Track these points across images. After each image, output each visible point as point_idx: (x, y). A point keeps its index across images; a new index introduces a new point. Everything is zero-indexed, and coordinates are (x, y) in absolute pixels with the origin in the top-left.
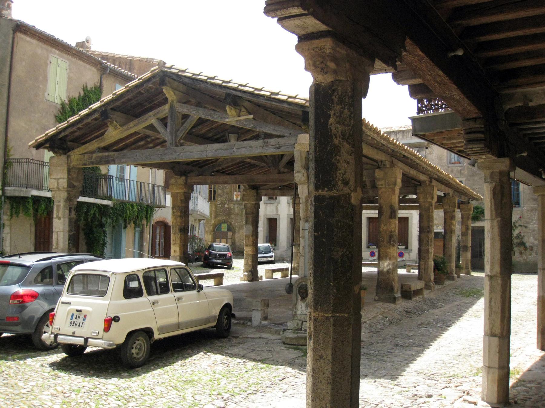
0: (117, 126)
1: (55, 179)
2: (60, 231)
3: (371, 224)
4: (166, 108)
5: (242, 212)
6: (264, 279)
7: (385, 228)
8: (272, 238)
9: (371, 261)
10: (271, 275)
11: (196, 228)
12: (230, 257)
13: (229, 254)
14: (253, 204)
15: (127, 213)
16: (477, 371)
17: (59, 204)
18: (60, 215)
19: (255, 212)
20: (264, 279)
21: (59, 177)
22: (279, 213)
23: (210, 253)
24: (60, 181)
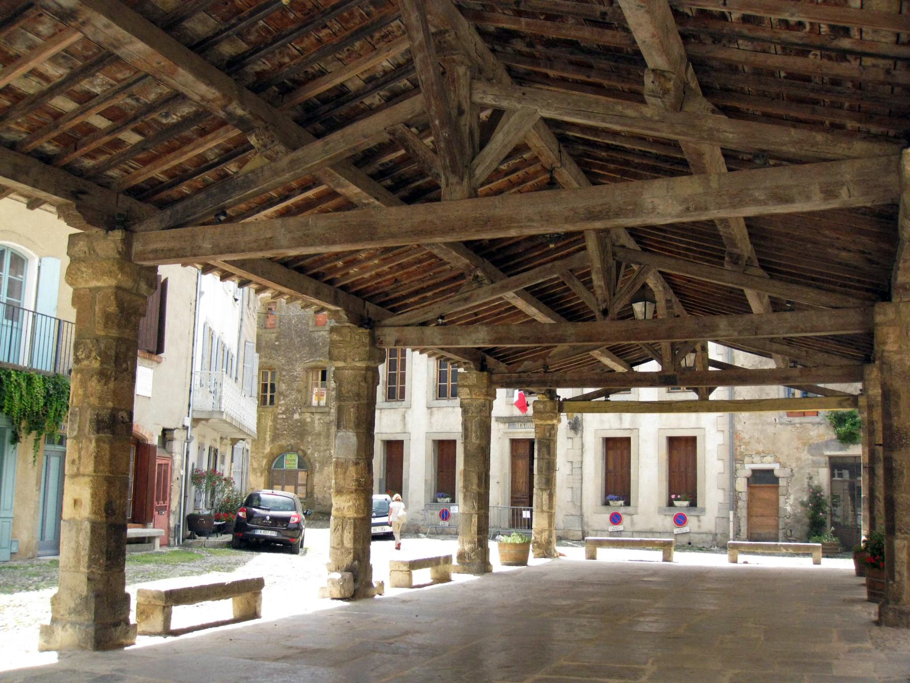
3: (611, 453)
5: (328, 430)
6: (390, 592)
8: (394, 484)
9: (612, 534)
10: (407, 577)
11: (223, 457)
12: (298, 523)
13: (295, 516)
14: (360, 369)
15: (11, 397)
19: (364, 392)
20: (390, 592)
22: (409, 428)
23: (250, 516)
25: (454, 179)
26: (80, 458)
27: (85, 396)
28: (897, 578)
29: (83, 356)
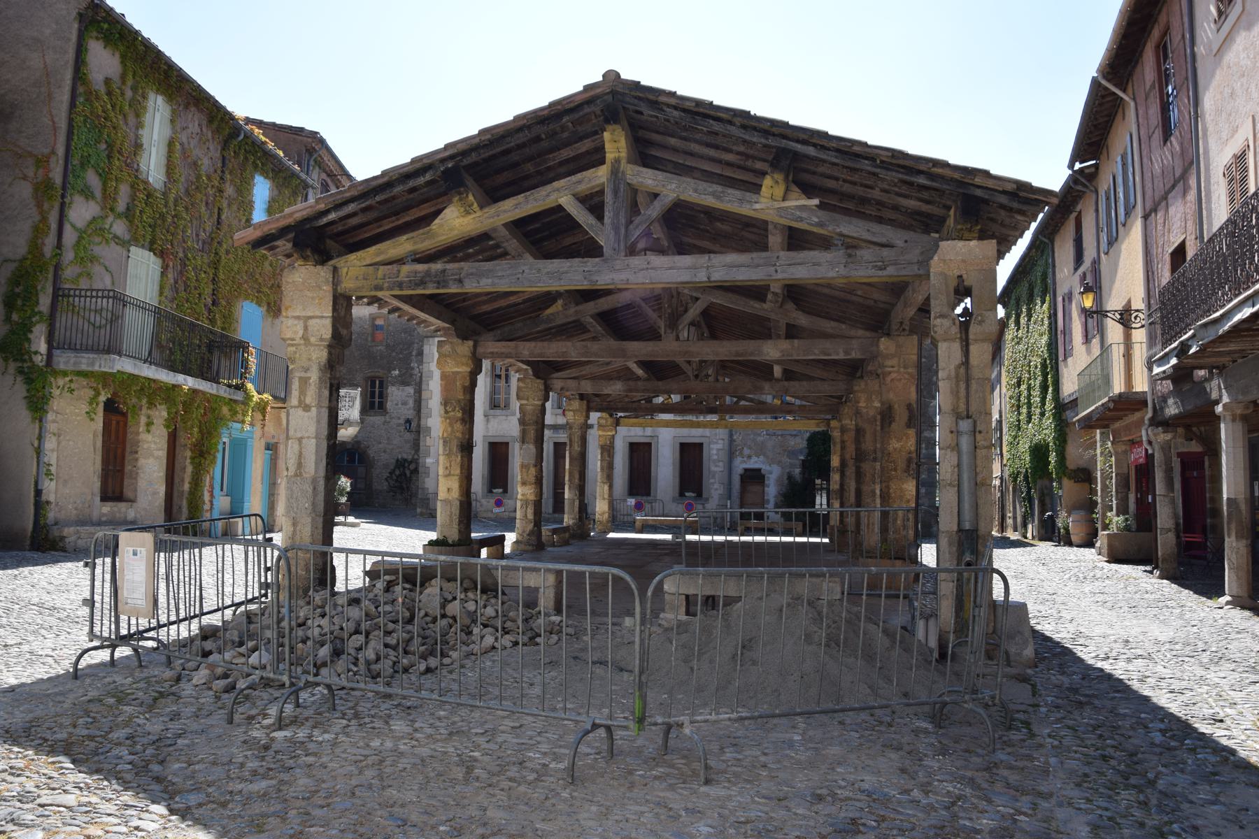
0: (472, 205)
1: (298, 318)
2: (308, 437)
4: (601, 175)
7: (897, 445)
17: (308, 375)
18: (308, 400)
21: (310, 314)
24: (311, 322)
25: (669, 331)
27: (453, 431)
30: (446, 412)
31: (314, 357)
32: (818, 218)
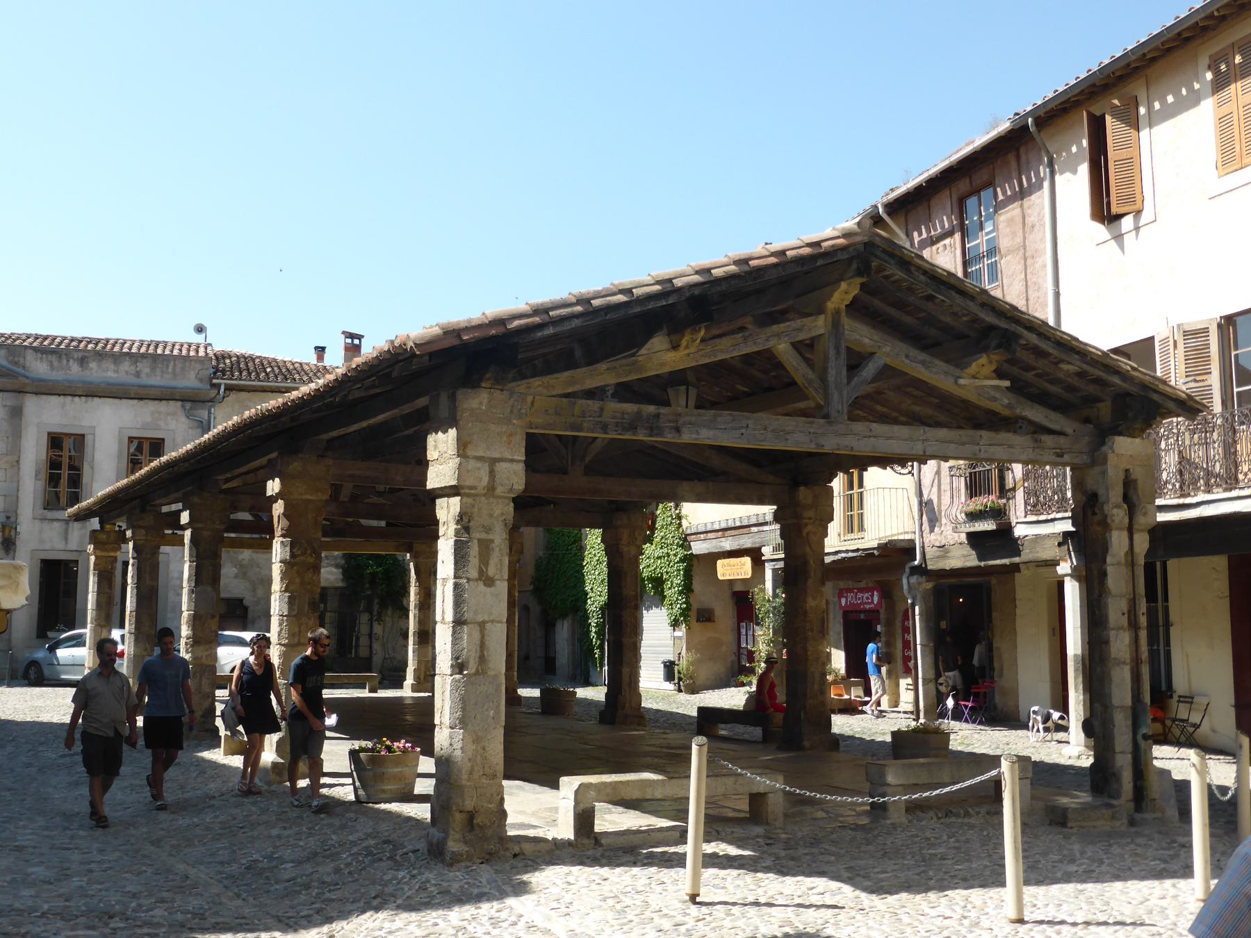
4: (819, 325)
16: (969, 855)
17: (491, 537)
21: (497, 455)
26: (300, 632)
28: (623, 693)
29: (299, 553)
30: (293, 555)
31: (497, 512)
32: (1009, 399)
